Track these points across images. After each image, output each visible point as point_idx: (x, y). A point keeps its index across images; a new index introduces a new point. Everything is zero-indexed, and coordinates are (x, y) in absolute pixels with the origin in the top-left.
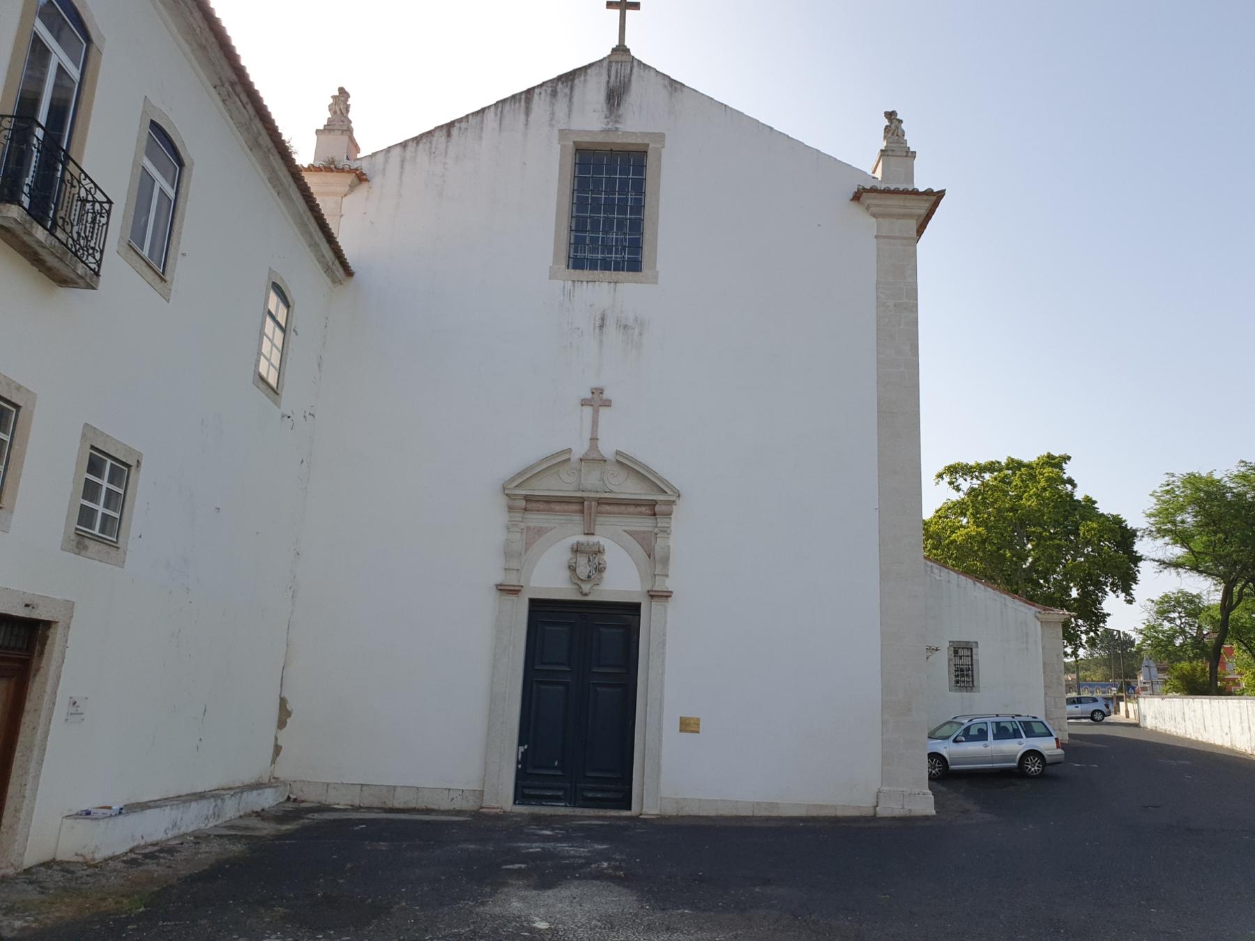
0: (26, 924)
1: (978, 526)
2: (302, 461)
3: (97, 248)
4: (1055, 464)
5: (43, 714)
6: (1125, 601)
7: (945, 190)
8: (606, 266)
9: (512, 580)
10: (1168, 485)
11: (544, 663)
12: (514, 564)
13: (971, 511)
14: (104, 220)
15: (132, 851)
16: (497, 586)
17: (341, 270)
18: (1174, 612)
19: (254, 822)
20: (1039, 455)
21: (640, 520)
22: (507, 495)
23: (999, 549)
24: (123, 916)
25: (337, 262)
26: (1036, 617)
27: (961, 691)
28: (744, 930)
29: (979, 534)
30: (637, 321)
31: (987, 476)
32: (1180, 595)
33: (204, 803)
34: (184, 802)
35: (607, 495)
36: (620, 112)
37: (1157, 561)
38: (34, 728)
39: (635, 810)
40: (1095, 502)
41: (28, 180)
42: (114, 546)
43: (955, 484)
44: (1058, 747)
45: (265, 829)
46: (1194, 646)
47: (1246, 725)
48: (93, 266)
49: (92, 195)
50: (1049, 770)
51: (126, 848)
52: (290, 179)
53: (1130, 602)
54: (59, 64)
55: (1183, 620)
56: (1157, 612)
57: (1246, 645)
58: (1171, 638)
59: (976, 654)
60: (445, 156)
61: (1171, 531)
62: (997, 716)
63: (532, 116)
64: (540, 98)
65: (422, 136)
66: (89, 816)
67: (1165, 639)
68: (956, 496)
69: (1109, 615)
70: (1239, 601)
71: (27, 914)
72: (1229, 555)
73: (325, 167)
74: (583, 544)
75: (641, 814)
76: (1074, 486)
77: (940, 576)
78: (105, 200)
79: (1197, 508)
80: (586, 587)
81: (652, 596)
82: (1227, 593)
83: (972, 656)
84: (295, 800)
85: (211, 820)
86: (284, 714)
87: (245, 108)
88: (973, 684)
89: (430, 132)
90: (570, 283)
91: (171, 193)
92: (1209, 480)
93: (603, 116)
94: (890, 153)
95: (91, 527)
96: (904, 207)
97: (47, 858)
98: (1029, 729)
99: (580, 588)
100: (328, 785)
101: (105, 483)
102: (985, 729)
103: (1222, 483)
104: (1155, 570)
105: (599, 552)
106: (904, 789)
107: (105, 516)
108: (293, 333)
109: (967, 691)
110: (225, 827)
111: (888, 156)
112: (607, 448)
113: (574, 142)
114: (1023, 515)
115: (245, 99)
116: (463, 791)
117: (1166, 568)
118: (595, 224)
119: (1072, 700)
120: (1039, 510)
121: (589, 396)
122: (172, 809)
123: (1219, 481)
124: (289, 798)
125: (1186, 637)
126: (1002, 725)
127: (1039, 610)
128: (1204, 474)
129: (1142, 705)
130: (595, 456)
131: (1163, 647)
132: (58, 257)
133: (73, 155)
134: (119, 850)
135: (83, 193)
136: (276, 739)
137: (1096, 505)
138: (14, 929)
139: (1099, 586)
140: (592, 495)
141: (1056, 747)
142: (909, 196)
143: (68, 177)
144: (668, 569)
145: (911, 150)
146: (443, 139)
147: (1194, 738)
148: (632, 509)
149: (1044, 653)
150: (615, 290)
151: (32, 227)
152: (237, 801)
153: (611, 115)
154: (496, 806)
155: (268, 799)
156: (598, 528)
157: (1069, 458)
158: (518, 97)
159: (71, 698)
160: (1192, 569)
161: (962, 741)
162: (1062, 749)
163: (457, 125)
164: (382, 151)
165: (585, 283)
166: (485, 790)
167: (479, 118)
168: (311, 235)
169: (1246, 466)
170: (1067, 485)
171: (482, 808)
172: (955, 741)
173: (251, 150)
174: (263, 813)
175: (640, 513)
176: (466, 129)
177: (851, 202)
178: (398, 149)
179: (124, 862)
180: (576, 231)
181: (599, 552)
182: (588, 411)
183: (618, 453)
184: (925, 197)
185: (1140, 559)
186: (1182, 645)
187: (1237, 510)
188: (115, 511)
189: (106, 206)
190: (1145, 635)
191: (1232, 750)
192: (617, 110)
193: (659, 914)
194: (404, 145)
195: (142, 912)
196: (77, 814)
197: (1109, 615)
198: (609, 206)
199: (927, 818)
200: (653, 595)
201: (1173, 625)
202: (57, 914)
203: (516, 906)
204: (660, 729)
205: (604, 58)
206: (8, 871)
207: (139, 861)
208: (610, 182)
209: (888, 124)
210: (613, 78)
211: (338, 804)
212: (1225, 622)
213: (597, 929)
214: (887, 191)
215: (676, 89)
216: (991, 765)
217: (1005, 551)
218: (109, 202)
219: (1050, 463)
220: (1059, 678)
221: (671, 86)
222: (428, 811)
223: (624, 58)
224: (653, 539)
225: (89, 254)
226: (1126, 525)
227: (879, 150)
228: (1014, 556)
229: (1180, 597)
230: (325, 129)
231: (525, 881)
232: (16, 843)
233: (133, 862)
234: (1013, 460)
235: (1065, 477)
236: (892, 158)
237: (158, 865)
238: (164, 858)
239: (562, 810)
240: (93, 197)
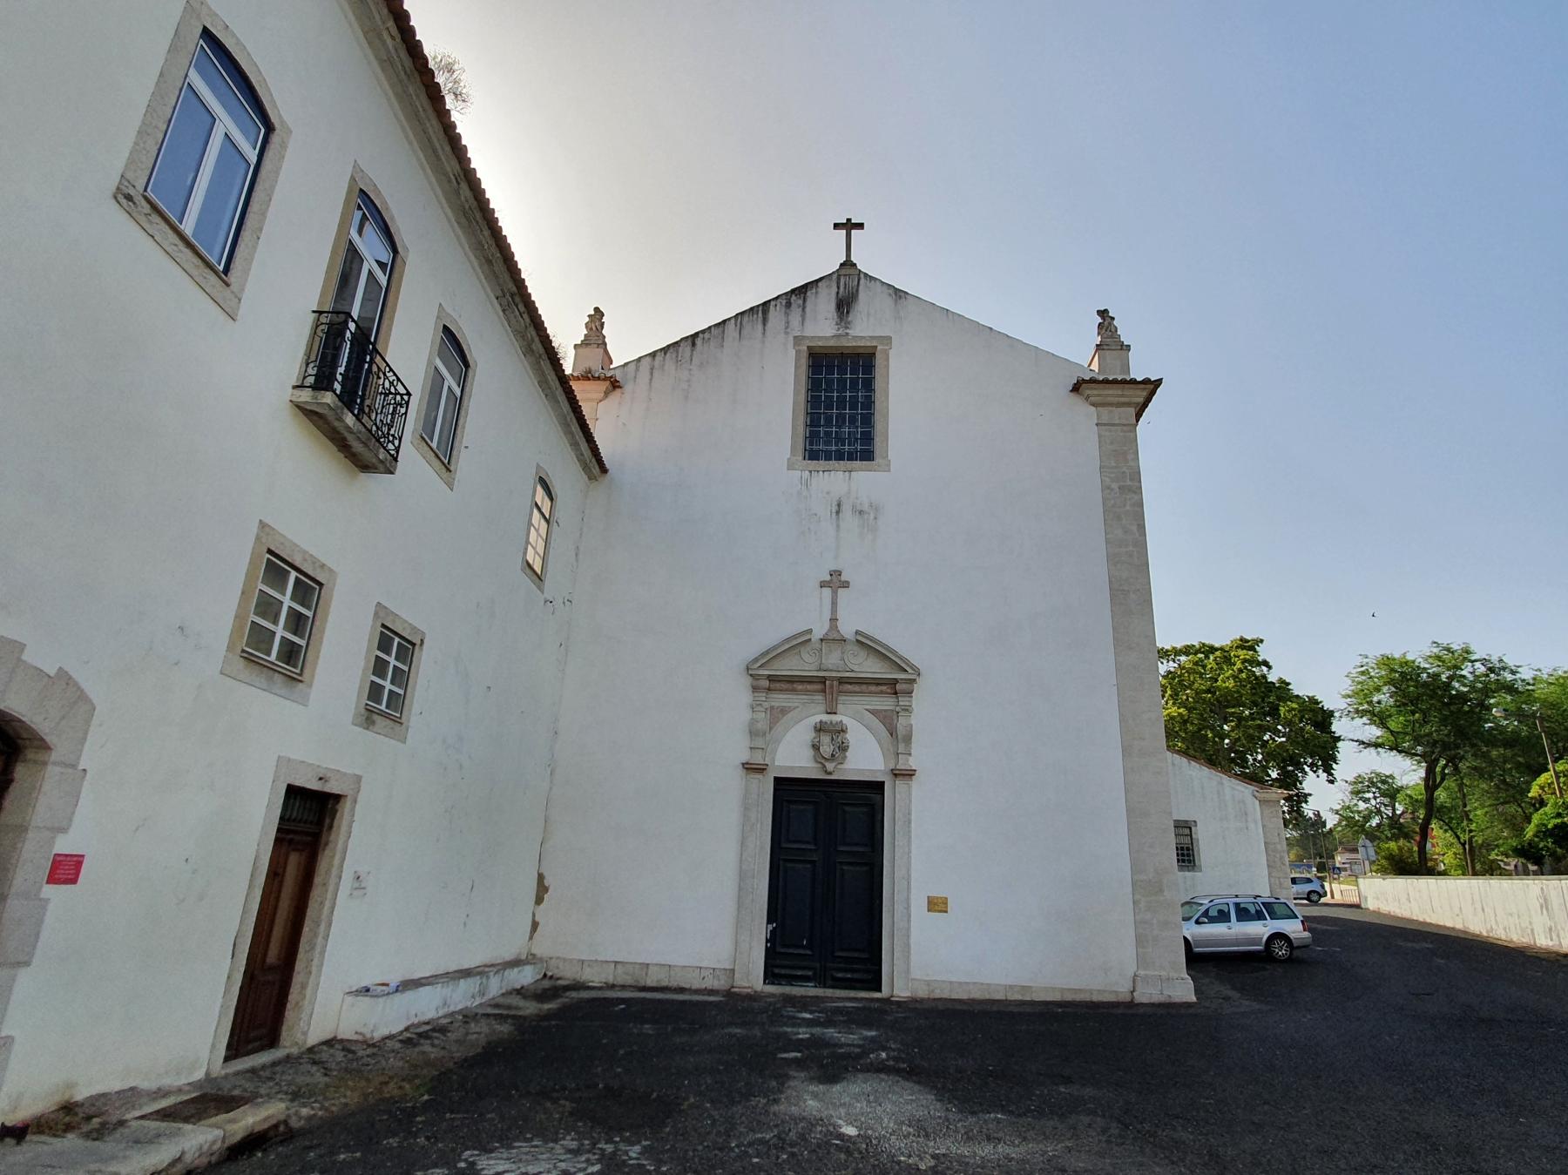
0: (312, 1112)
1: (1179, 708)
2: (561, 645)
3: (396, 435)
4: (1249, 646)
5: (331, 888)
6: (1327, 780)
7: (1162, 379)
8: (840, 456)
9: (758, 759)
10: (1362, 666)
11: (790, 842)
12: (759, 743)
13: (1169, 692)
14: (403, 410)
15: (407, 1029)
16: (743, 764)
17: (597, 467)
18: (1368, 792)
19: (516, 1001)
20: (1232, 639)
22: (751, 675)
23: (1200, 730)
24: (408, 1105)
25: (594, 460)
26: (1254, 796)
28: (1071, 1141)
29: (1180, 714)
31: (1183, 658)
32: (1373, 775)
33: (470, 981)
34: (453, 979)
35: (847, 674)
36: (850, 319)
37: (1356, 741)
38: (321, 903)
39: (885, 992)
40: (1289, 684)
41: (341, 370)
42: (398, 721)
44: (1305, 930)
45: (528, 1008)
46: (1391, 827)
47: (1479, 906)
48: (392, 452)
49: (395, 387)
50: (1296, 953)
51: (402, 1027)
52: (557, 382)
53: (1332, 782)
54: (370, 270)
55: (1378, 800)
56: (1352, 793)
57: (1447, 824)
58: (1367, 818)
60: (691, 363)
61: (1369, 711)
62: (1237, 896)
63: (769, 325)
64: (776, 310)
65: (669, 346)
66: (369, 994)
67: (1361, 819)
69: (1310, 795)
70: (1443, 779)
71: (313, 1100)
72: (1430, 734)
73: (582, 376)
74: (826, 723)
75: (892, 996)
76: (1269, 667)
78: (405, 392)
79: (1393, 689)
80: (830, 766)
81: (896, 775)
82: (1430, 771)
83: (1191, 836)
84: (551, 977)
85: (477, 999)
86: (542, 889)
87: (522, 317)
88: (1194, 863)
89: (676, 343)
91: (458, 392)
92: (1404, 660)
94: (1105, 347)
95: (379, 703)
96: (1122, 396)
97: (328, 1036)
98: (1270, 910)
99: (825, 766)
100: (583, 961)
101: (392, 661)
102: (1226, 911)
103: (1417, 664)
104: (1355, 750)
105: (843, 731)
107: (391, 691)
108: (555, 524)
110: (490, 1005)
111: (1103, 349)
112: (847, 629)
113: (808, 347)
114: (1221, 696)
115: (522, 308)
116: (714, 969)
117: (1365, 748)
118: (829, 420)
119: (280, 871)
120: (1238, 692)
121: (828, 578)
122: (443, 987)
123: (1414, 662)
124: (545, 975)
125: (1382, 817)
126: (1242, 906)
127: (1256, 789)
128: (1396, 656)
129: (1361, 886)
130: (835, 636)
131: (1355, 826)
132: (363, 443)
133: (379, 347)
134: (396, 1028)
135: (387, 384)
136: (534, 915)
137: (1290, 687)
138: (300, 1118)
139: (1299, 766)
140: (834, 674)
142: (1127, 386)
143: (375, 369)
144: (911, 748)
145: (1125, 343)
146: (688, 349)
147: (1421, 920)
148: (873, 688)
150: (850, 476)
151: (342, 413)
152: (500, 979)
154: (747, 985)
155: (526, 977)
157: (1262, 641)
158: (755, 309)
159: (355, 872)
160: (1391, 749)
161: (1205, 923)
163: (701, 335)
164: (634, 361)
165: (821, 473)
166: (736, 968)
167: (721, 329)
168: (572, 433)
169: (1438, 647)
171: (733, 987)
172: (1197, 922)
173: (525, 355)
174: (523, 991)
175: (882, 692)
176: (709, 339)
177: (1072, 394)
178: (648, 359)
179: (401, 1041)
180: (811, 426)
181: (843, 731)
182: (827, 592)
183: (857, 632)
184: (1142, 386)
185: (1338, 739)
186: (1379, 825)
187: (1433, 690)
188: (399, 687)
189: (406, 398)
190: (1340, 815)
191: (1465, 932)
192: (847, 317)
193: (972, 1120)
194: (653, 355)
195: (427, 1101)
196: (357, 991)
197: (1310, 795)
198: (841, 403)
199: (1188, 1005)
200: (896, 774)
201: (1368, 805)
202: (343, 1100)
203: (812, 1105)
204: (908, 908)
205: (833, 273)
206: (292, 1050)
207: (415, 1041)
208: (842, 382)
209: (1101, 321)
211: (592, 982)
212: (1430, 802)
213: (911, 1137)
214: (1106, 381)
215: (900, 297)
217: (1206, 732)
218: (409, 394)
221: (896, 295)
222: (681, 990)
223: (851, 271)
224: (895, 717)
225: (389, 441)
226: (1323, 706)
227: (1094, 345)
228: (1215, 736)
229: (1373, 778)
230: (582, 344)
231: (806, 1073)
232: (302, 1021)
233: (408, 1042)
234: (1203, 644)
235: (1260, 659)
236: (1108, 352)
237: (433, 1045)
238: (437, 1038)
239: (810, 991)
240: (396, 389)
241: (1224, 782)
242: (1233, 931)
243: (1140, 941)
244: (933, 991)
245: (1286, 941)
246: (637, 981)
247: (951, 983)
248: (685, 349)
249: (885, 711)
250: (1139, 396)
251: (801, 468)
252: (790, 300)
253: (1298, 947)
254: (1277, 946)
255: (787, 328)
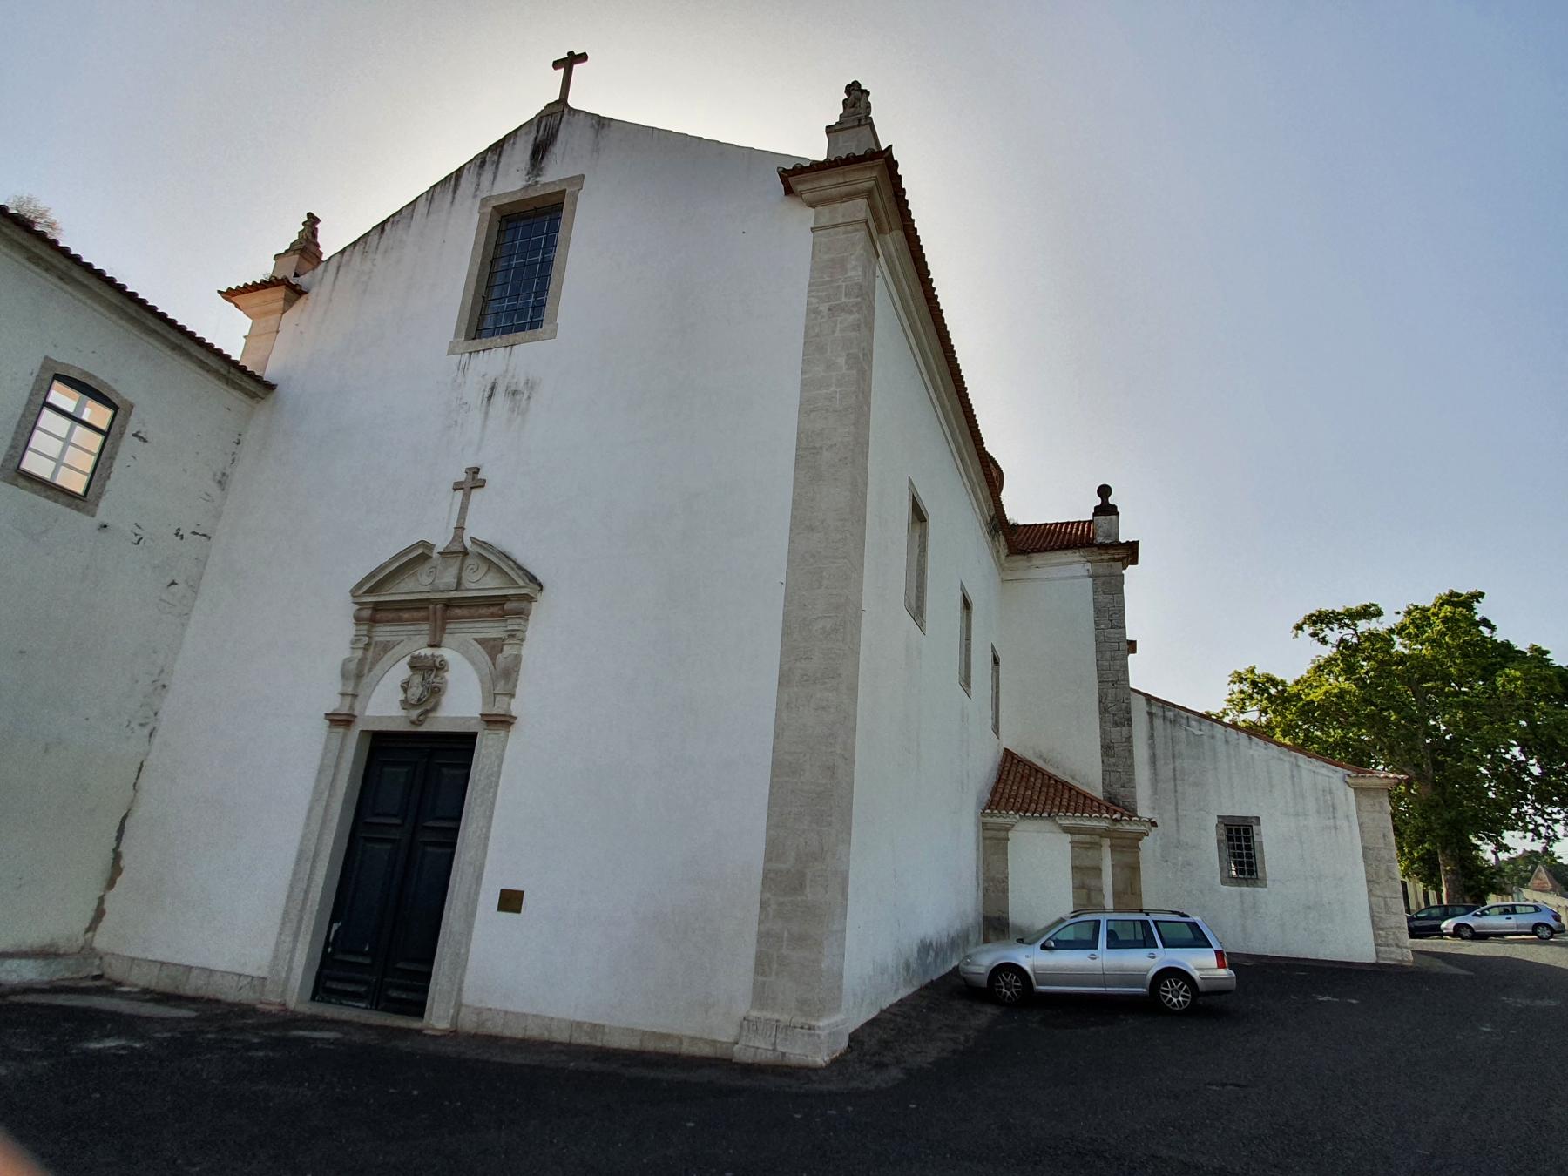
11: (378, 815)
16: (326, 714)
21: (492, 624)
23: (1382, 710)
26: (1346, 782)
27: (1239, 885)
30: (527, 383)
40: (1547, 652)
43: (1320, 636)
44: (1221, 966)
50: (1200, 1001)
59: (1257, 834)
68: (1328, 651)
76: (1493, 628)
77: (1200, 730)
90: (467, 355)
93: (525, 173)
96: (845, 184)
106: (781, 1018)
109: (1247, 886)
127: (1349, 772)
137: (1548, 656)
141: (1216, 966)
148: (483, 611)
149: (1362, 832)
153: (533, 170)
156: (447, 639)
157: (1482, 595)
162: (1231, 967)
170: (1481, 628)
172: (1044, 947)
192: (541, 162)
209: (846, 97)
210: (541, 132)
216: (1103, 989)
219: (1453, 602)
220: (1388, 870)
235: (1477, 618)
241: (1301, 763)
242: (1097, 963)
243: (762, 963)
244: (483, 1023)
245: (1185, 982)
246: (177, 987)
247: (506, 1013)
248: (375, 237)
249: (494, 639)
250: (866, 180)
251: (461, 351)
252: (485, 158)
253: (1207, 994)
254: (1170, 989)
255: (476, 190)
